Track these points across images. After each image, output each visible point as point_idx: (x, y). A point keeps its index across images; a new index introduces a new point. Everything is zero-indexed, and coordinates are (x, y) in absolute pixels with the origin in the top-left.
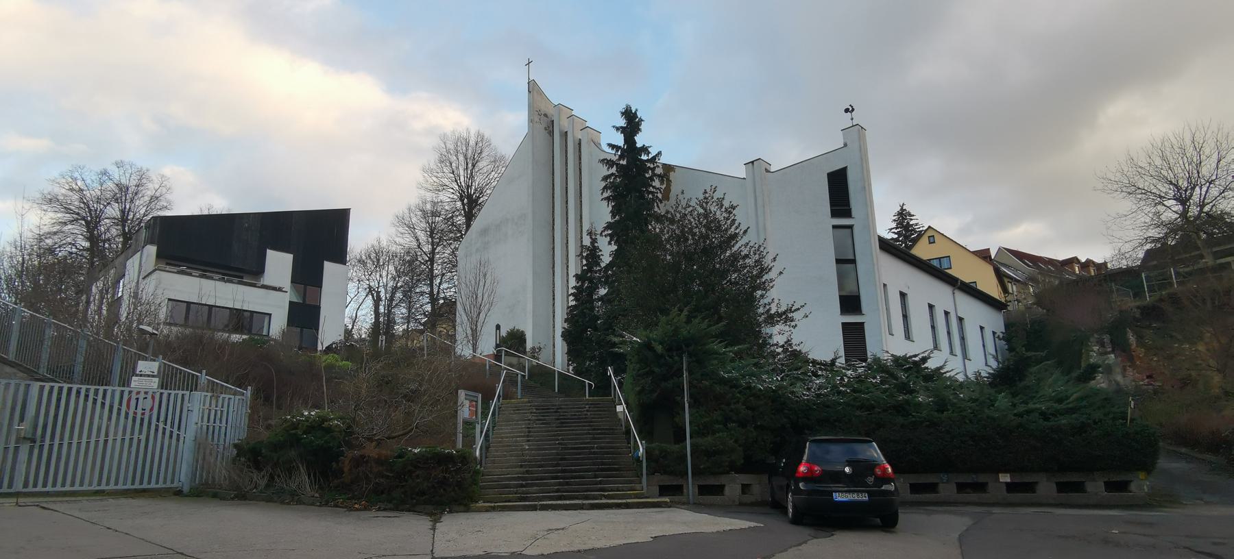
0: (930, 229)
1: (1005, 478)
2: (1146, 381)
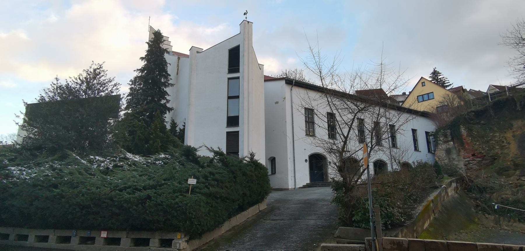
1: (104, 234)
2: (471, 158)
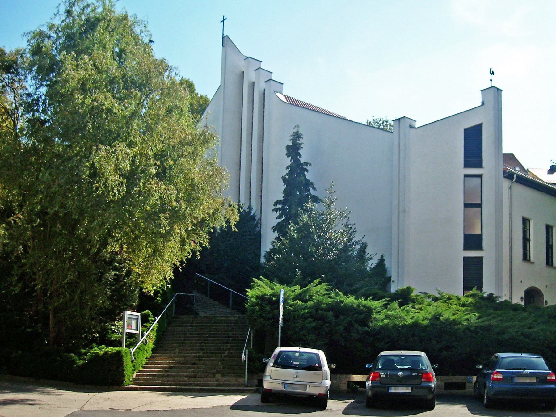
0: (382, 382)
